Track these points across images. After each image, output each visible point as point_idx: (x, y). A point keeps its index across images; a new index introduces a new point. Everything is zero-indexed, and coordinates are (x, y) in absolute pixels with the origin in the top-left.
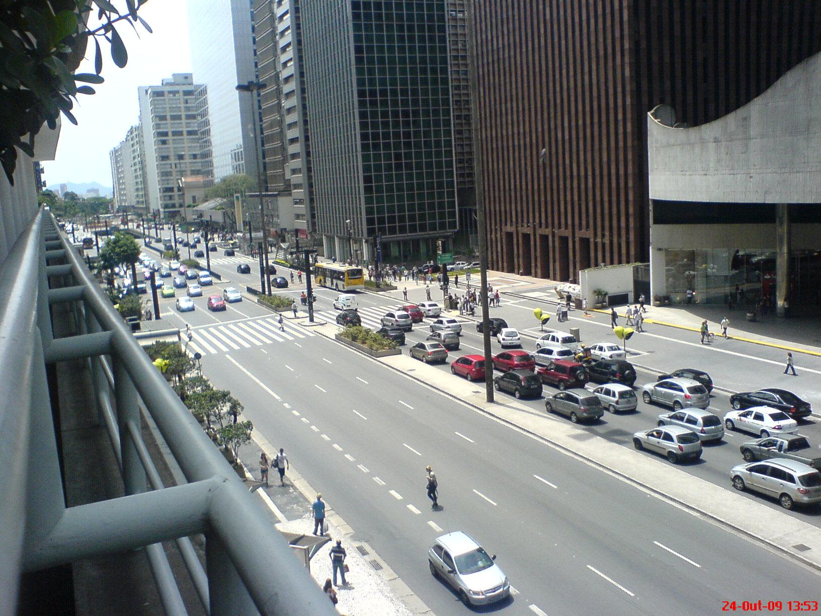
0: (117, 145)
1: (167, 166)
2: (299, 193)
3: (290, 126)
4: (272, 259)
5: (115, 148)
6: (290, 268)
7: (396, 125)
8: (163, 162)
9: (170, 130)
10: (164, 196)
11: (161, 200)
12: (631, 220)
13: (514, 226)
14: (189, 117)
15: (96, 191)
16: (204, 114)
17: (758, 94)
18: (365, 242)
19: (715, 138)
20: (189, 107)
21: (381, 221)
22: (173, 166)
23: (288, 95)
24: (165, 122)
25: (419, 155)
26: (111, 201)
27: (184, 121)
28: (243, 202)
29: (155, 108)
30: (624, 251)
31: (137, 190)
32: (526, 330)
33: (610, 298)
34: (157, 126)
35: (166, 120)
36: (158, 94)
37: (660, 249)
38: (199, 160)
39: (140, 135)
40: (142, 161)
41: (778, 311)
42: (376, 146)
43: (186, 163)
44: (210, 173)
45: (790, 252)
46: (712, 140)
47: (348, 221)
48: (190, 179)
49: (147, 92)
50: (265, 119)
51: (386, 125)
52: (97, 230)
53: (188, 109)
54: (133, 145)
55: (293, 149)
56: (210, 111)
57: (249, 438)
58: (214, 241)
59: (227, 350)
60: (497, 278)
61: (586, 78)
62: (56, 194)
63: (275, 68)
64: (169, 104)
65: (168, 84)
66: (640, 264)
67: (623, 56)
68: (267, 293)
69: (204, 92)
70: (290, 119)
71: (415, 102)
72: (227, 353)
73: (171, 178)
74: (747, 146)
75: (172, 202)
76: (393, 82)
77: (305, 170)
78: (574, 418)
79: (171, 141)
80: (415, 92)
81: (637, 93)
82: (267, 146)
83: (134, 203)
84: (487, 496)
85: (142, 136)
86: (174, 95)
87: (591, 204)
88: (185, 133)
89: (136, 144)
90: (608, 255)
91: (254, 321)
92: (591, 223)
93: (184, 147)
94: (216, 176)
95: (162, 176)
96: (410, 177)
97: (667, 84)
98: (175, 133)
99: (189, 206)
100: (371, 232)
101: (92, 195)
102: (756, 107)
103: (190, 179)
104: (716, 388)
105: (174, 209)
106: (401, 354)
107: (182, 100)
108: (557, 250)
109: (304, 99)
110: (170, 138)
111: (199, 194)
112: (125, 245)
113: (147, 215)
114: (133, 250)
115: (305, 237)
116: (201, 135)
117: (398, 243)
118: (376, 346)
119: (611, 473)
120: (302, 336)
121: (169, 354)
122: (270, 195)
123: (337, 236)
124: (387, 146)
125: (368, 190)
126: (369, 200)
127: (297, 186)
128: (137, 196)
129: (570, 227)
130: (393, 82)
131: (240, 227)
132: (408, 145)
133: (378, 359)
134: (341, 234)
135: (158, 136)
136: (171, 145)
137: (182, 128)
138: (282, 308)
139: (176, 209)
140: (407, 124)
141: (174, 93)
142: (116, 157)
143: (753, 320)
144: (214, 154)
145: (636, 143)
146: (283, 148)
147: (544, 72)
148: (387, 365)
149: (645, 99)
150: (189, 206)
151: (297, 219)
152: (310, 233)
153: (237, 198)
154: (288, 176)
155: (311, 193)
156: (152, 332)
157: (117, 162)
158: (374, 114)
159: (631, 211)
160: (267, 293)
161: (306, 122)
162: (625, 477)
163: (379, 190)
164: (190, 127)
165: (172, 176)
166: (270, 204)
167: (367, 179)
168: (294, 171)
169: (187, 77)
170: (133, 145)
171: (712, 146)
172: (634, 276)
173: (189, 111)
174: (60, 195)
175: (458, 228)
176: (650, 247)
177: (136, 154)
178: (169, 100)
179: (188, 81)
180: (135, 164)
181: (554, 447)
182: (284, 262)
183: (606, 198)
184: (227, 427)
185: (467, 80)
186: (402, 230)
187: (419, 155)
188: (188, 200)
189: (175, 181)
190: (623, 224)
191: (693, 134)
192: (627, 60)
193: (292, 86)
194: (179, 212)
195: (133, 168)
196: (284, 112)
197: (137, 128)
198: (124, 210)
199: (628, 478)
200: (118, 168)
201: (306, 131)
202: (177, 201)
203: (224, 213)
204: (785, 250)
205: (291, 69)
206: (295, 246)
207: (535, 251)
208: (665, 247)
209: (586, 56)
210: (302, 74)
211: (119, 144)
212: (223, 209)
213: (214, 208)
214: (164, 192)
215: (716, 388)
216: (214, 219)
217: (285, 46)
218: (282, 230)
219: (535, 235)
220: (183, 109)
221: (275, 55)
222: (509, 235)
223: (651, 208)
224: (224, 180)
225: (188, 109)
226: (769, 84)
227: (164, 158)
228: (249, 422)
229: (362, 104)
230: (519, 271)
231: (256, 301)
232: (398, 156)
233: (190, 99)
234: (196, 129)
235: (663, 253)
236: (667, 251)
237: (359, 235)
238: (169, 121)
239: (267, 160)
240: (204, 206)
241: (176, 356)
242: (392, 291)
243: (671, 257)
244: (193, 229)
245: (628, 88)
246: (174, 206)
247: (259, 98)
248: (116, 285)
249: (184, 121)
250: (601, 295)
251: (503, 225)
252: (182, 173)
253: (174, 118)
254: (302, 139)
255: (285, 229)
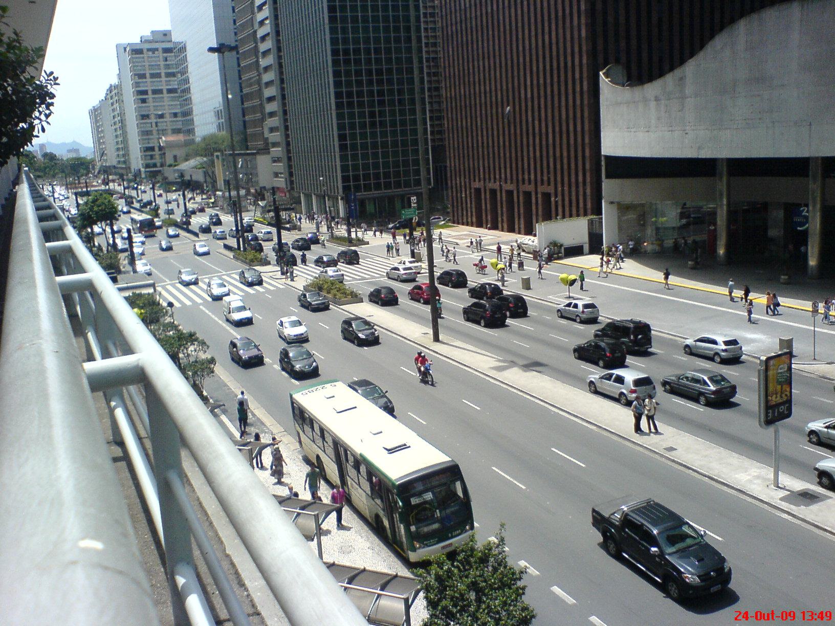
0: (95, 103)
1: (148, 125)
2: (277, 151)
3: (268, 84)
4: (247, 218)
5: (94, 107)
6: (268, 225)
7: (370, 82)
8: (144, 121)
9: (149, 89)
10: (146, 156)
11: (142, 159)
12: (588, 175)
13: (482, 182)
14: (168, 75)
15: (77, 151)
16: (184, 72)
17: (692, 55)
18: (341, 199)
19: (656, 97)
20: (168, 65)
21: (356, 178)
22: (154, 125)
23: (265, 53)
24: (144, 80)
25: (393, 113)
26: (92, 161)
27: (164, 79)
28: (223, 160)
29: (134, 66)
30: (581, 205)
31: (118, 149)
32: (550, 297)
33: (565, 249)
34: (137, 84)
35: (146, 78)
36: (136, 51)
37: (612, 203)
38: (180, 119)
39: (119, 94)
40: (122, 120)
41: (810, 272)
42: (350, 105)
43: (166, 122)
44: (191, 131)
45: (729, 204)
46: (653, 99)
47: (321, 178)
48: (172, 138)
49: (125, 49)
50: (244, 78)
51: (359, 83)
52: (77, 191)
53: (167, 67)
54: (112, 104)
55: (270, 107)
56: (191, 69)
57: (213, 372)
58: (194, 200)
59: (201, 301)
60: (465, 233)
61: (547, 37)
62: (35, 154)
63: (252, 25)
64: (149, 62)
65: (147, 41)
66: (595, 217)
67: (579, 17)
68: (242, 249)
69: (183, 49)
70: (267, 77)
71: (389, 61)
72: (201, 304)
73: (152, 137)
74: (683, 105)
75: (153, 161)
76: (367, 41)
77: (282, 128)
78: (623, 401)
79: (151, 100)
80: (388, 51)
81: (593, 54)
82: (246, 105)
83: (114, 163)
84: (419, 418)
85: (122, 95)
86: (154, 53)
87: (551, 160)
88: (165, 91)
89: (115, 103)
90: (567, 209)
91: (229, 275)
92: (552, 179)
93: (164, 106)
94: (197, 134)
95: (142, 135)
96: (384, 134)
97: (623, 44)
98: (155, 92)
99: (170, 166)
100: (346, 189)
101: (74, 155)
102: (690, 68)
103: (172, 138)
104: (602, 316)
105: (155, 169)
106: (362, 302)
107: (161, 58)
108: (504, 203)
109: (280, 57)
110: (150, 96)
111: (180, 153)
112: (103, 203)
113: (127, 175)
114: (111, 208)
115: (284, 195)
116: (182, 92)
117: (374, 199)
118: (339, 295)
119: (528, 397)
120: (272, 288)
121: (143, 303)
122: (248, 154)
123: (314, 194)
124: (361, 104)
125: (343, 147)
126: (343, 158)
127: (275, 145)
128: (118, 155)
129: (552, 183)
130: (367, 41)
131: (221, 186)
132: (382, 103)
133: (341, 307)
134: (318, 191)
135: (137, 95)
136: (150, 103)
137: (162, 86)
138: (256, 263)
139: (157, 169)
140: (380, 82)
141: (154, 50)
142: (96, 117)
143: (693, 268)
144: (194, 113)
145: (592, 101)
146: (262, 106)
147: (508, 32)
148: (348, 312)
149: (601, 59)
150: (170, 166)
151: (276, 177)
152: (289, 191)
153: (217, 156)
154: (266, 134)
155: (289, 151)
156: (129, 285)
157: (97, 121)
158: (348, 74)
159: (588, 166)
160: (242, 249)
161: (282, 81)
162: (540, 400)
163: (354, 147)
164: (170, 85)
165: (152, 135)
166: (249, 163)
167: (342, 137)
168: (272, 130)
169: (166, 34)
170: (112, 104)
171: (653, 104)
172: (589, 229)
173: (169, 68)
174: (39, 156)
175: (432, 185)
176: (603, 201)
177: (116, 113)
178: (148, 57)
179: (167, 38)
180: (115, 123)
181: (485, 377)
182: (262, 220)
183: (565, 154)
184: (192, 362)
185: (435, 37)
186: (378, 187)
187: (393, 113)
188: (169, 160)
189: (156, 141)
190: (580, 179)
191: (652, 89)
192: (583, 21)
193: (268, 44)
194: (160, 171)
195: (113, 128)
196: (262, 71)
197: (116, 87)
198: (106, 170)
199: (542, 401)
200: (98, 127)
201: (283, 89)
202: (158, 160)
203: (205, 172)
204: (725, 202)
205: (267, 29)
206: (272, 204)
207: (502, 207)
208: (617, 200)
209: (546, 18)
210: (278, 33)
211: (98, 102)
212: (204, 168)
213: (195, 167)
214: (144, 151)
215: (602, 316)
216: (194, 178)
217: (261, 4)
218: (261, 188)
219: (536, 193)
220: (162, 66)
221: (253, 13)
222: (478, 191)
223: (603, 163)
224: (204, 139)
225: (167, 67)
226: (702, 46)
227: (144, 117)
228: (212, 358)
229: (335, 63)
230: (487, 225)
231: (232, 257)
232: (372, 115)
233: (170, 56)
234: (177, 87)
235: (615, 207)
236: (619, 203)
237: (335, 193)
238: (148, 80)
239: (247, 118)
240: (184, 166)
241: (150, 305)
242: (363, 246)
243: (623, 208)
244: (174, 188)
245: (584, 48)
246: (155, 165)
247: (238, 56)
248: (96, 244)
249: (164, 79)
250: (557, 246)
251: (472, 181)
252: (164, 132)
253: (153, 76)
254: (279, 98)
255: (264, 187)
